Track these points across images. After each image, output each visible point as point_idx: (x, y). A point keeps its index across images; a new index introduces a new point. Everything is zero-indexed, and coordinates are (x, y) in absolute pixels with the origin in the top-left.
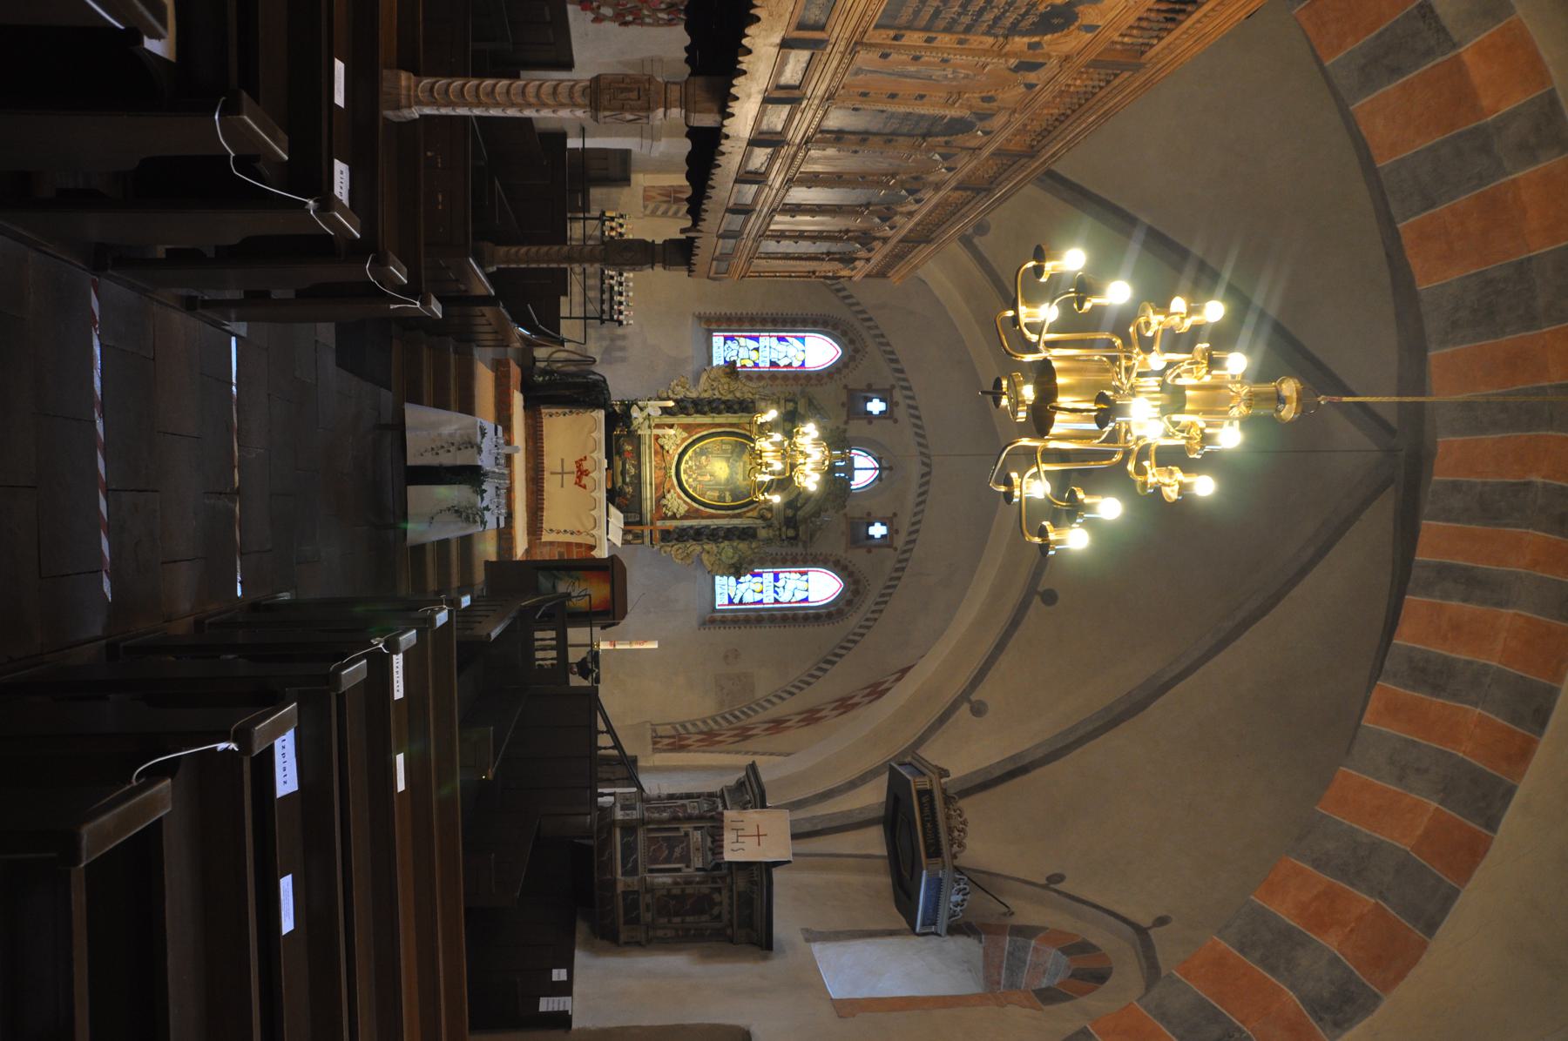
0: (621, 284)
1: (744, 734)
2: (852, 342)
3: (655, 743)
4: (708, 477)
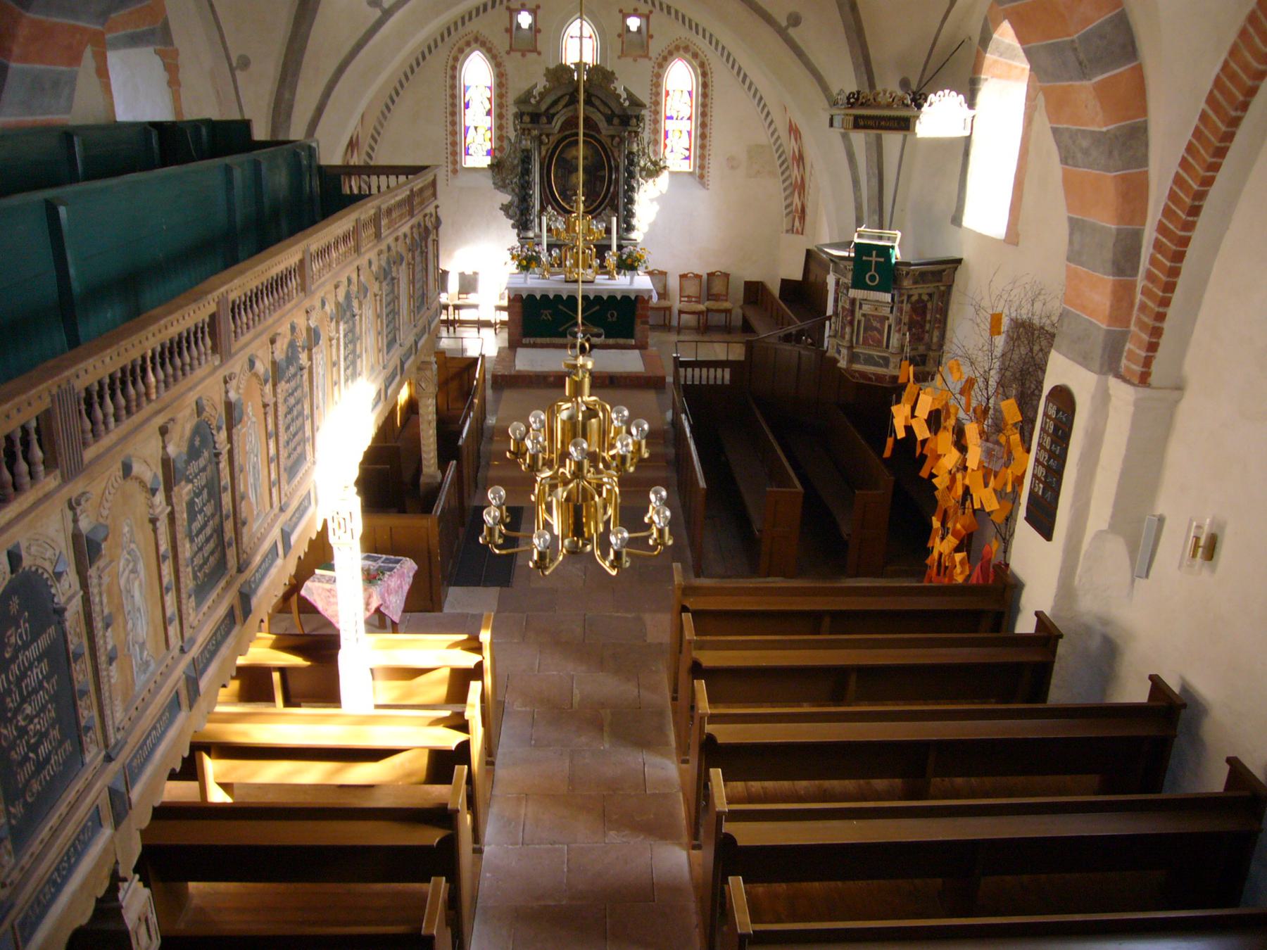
2: (468, 44)
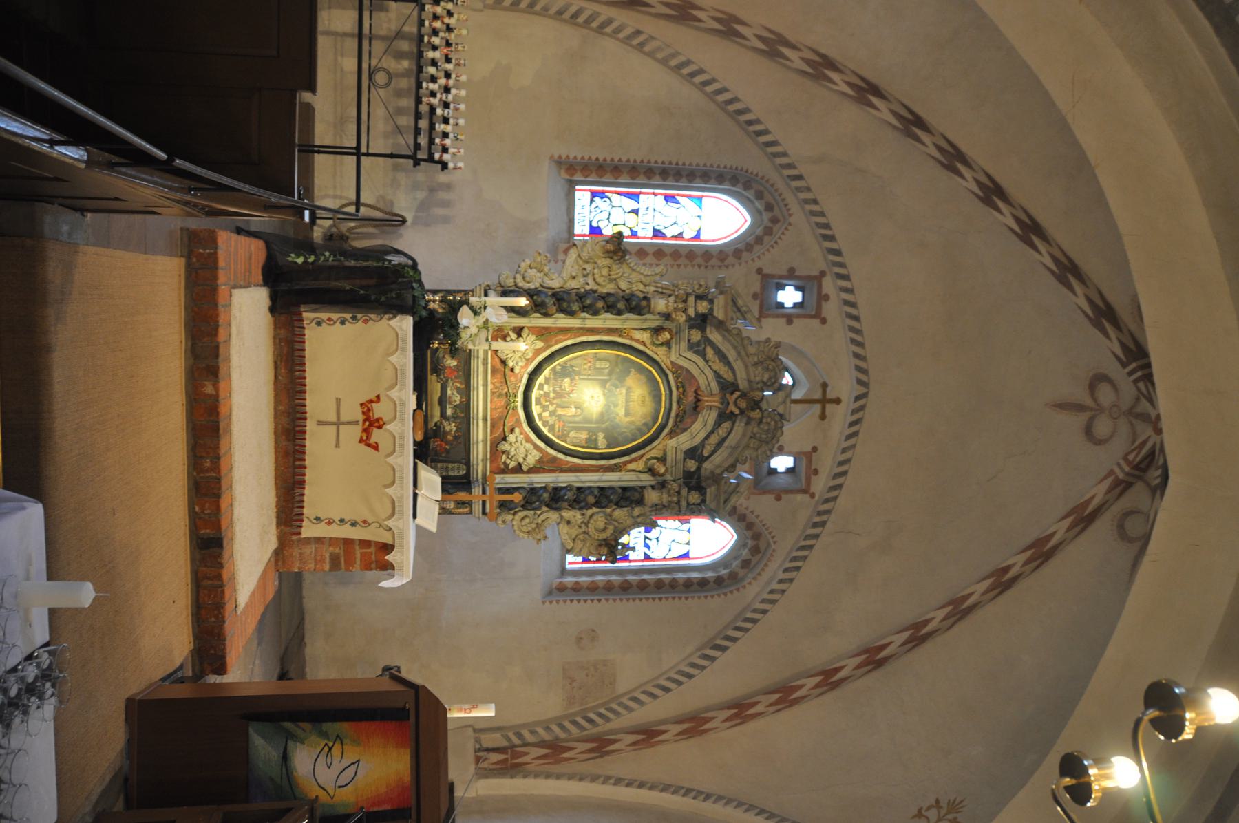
0: (446, 105)
1: (601, 746)
4: (572, 411)
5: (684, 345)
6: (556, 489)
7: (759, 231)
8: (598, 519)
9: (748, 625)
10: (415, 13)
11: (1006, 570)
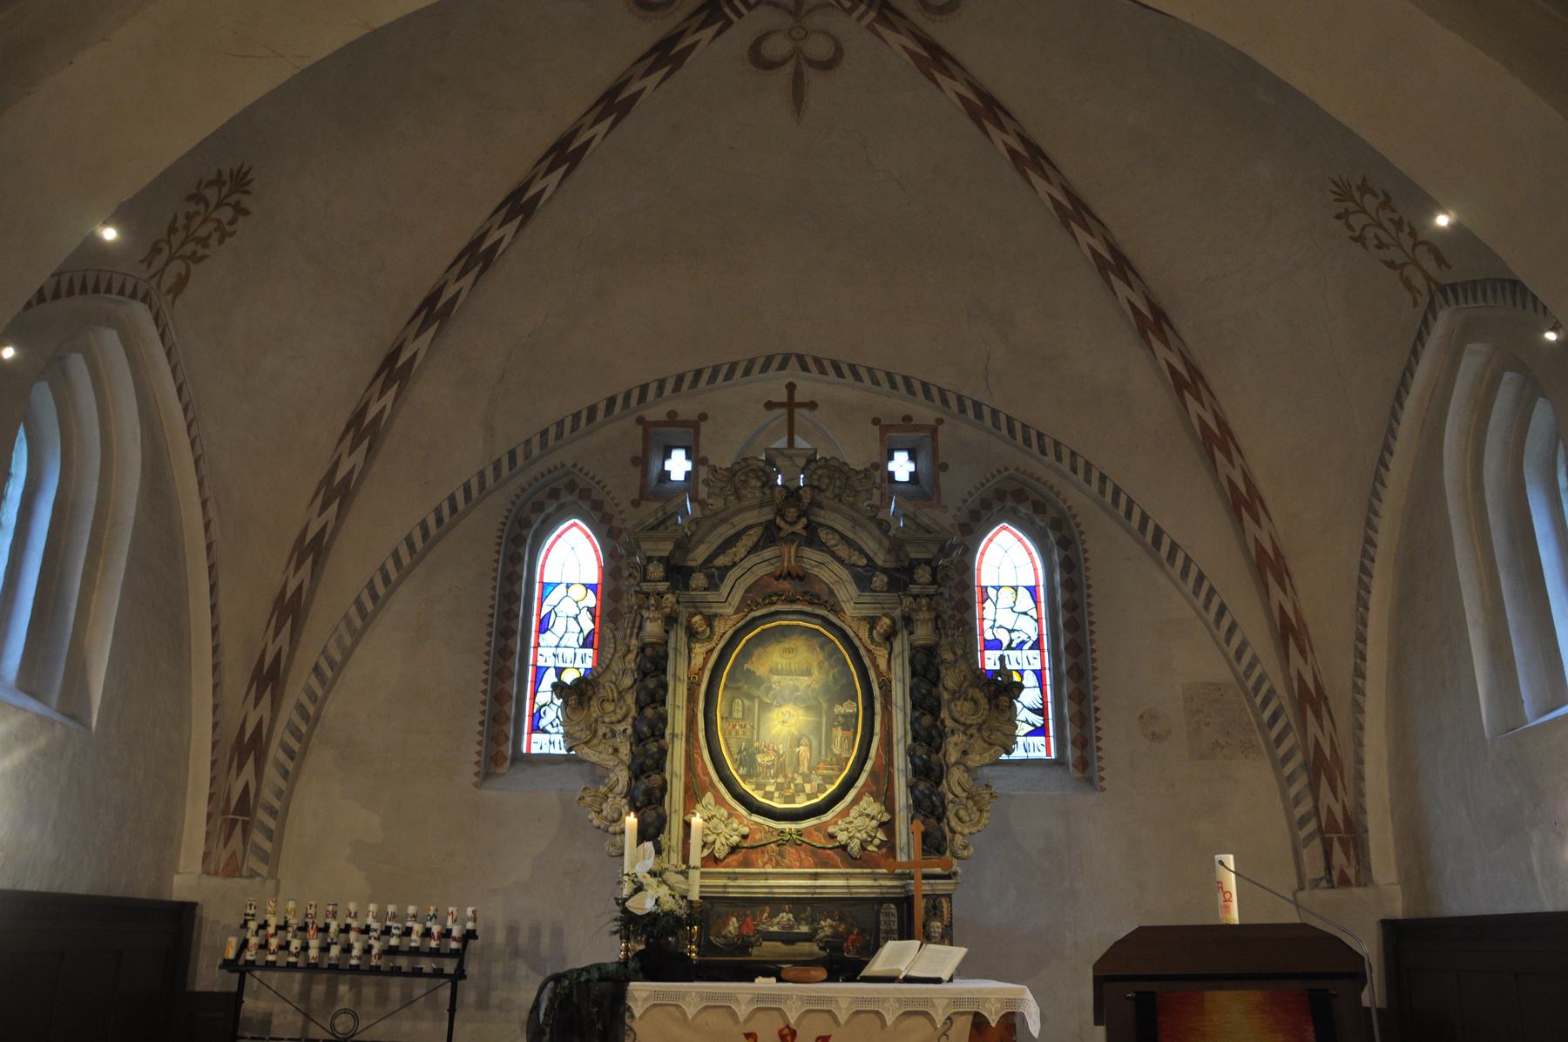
0: (387, 931)
1: (1311, 700)
3: (1345, 882)
5: (711, 596)
6: (915, 772)
7: (586, 506)
8: (955, 712)
9: (1123, 500)
10: (257, 973)
11: (1013, 153)
